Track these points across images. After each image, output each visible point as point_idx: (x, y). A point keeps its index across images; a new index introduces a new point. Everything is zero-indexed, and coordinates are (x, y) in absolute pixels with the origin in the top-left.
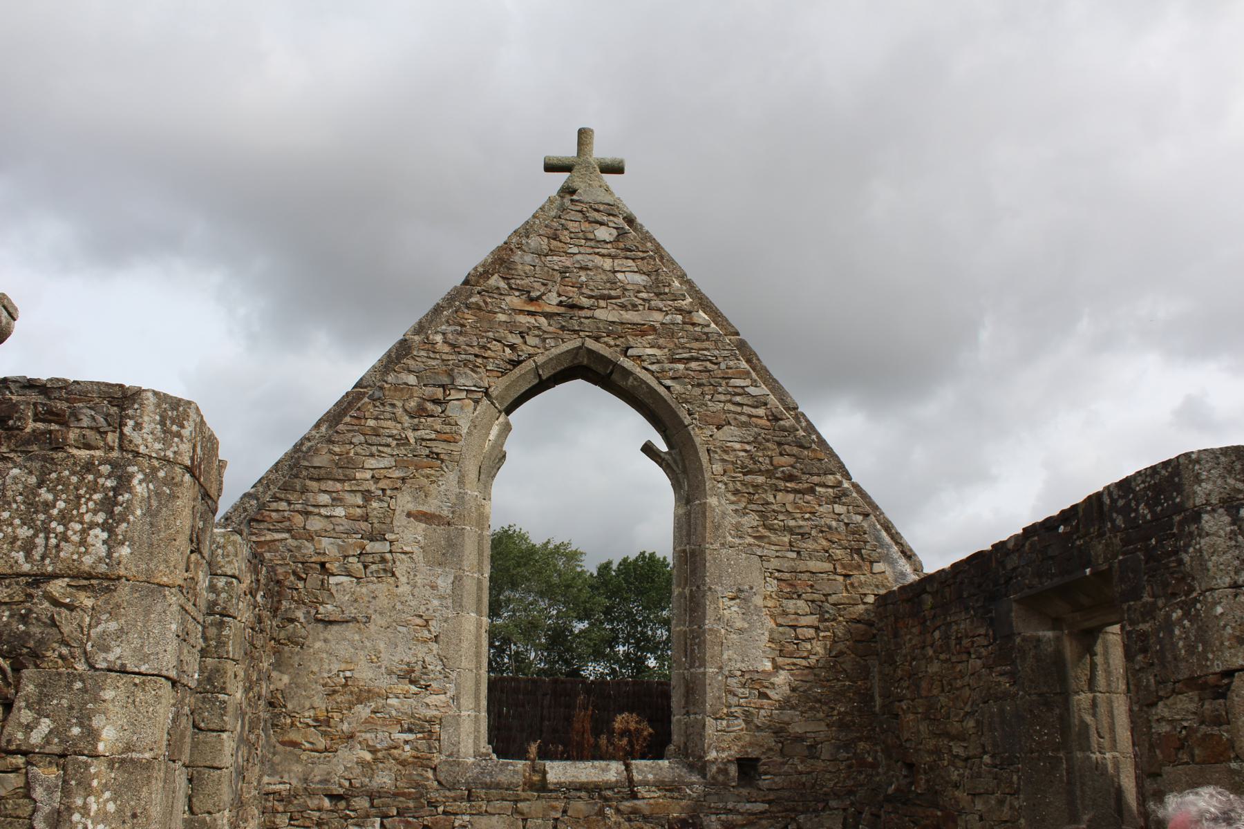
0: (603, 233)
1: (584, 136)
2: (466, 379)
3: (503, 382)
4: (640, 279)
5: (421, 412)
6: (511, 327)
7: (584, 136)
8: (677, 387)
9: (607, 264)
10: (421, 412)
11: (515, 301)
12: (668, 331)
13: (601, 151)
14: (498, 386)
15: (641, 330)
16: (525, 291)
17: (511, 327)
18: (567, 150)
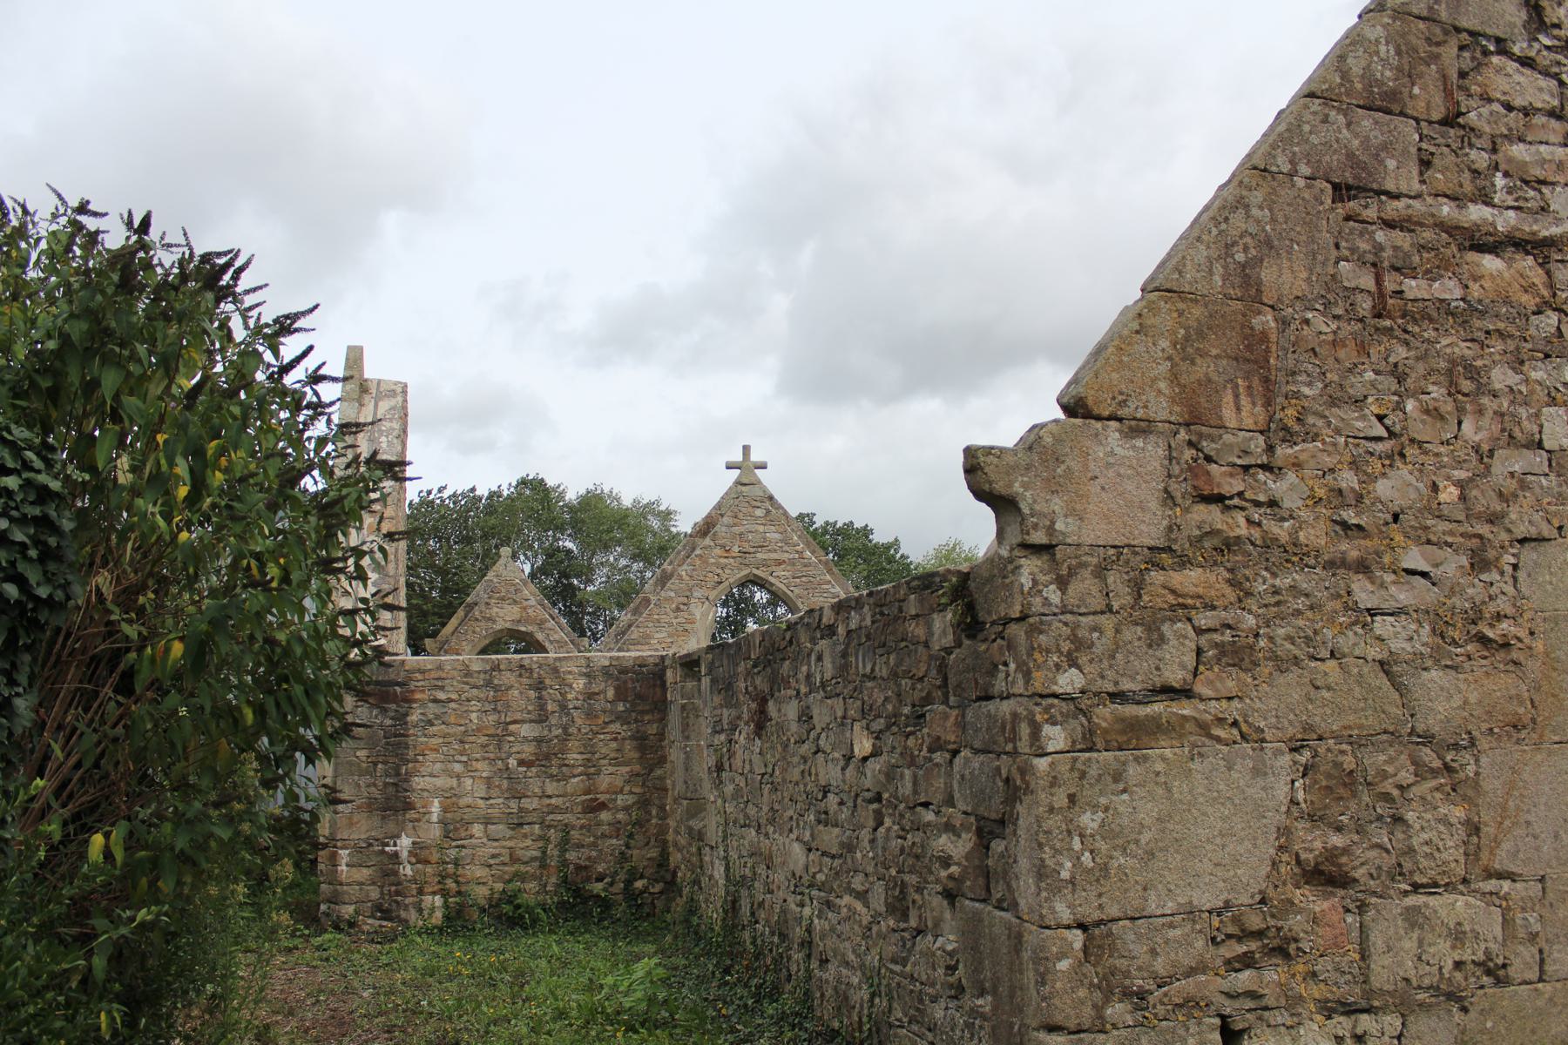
0: (759, 513)
1: (746, 450)
2: (697, 593)
3: (715, 593)
4: (777, 536)
5: (678, 609)
6: (717, 565)
7: (746, 450)
8: (796, 591)
9: (761, 528)
10: (678, 609)
11: (718, 551)
12: (792, 562)
13: (755, 457)
14: (713, 595)
15: (779, 563)
16: (723, 547)
17: (717, 565)
18: (738, 457)
